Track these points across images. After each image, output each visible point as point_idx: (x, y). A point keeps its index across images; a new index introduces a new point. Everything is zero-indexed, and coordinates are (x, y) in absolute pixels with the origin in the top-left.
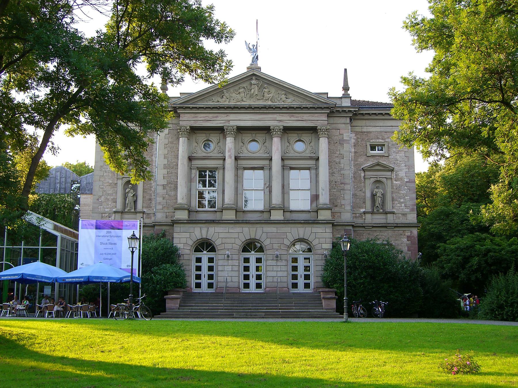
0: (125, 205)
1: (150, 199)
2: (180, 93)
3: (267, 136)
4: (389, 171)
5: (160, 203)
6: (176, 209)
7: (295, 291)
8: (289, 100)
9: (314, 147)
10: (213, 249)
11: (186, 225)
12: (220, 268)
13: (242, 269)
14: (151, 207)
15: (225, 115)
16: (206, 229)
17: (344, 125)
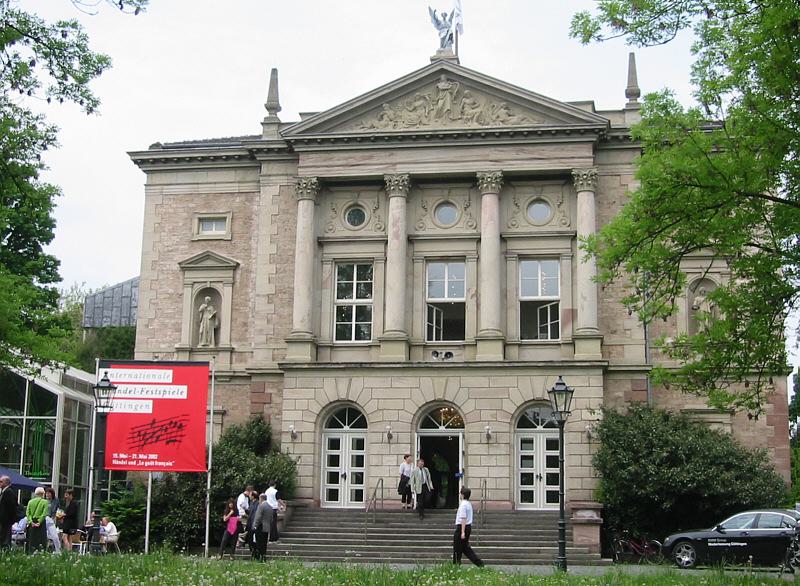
0: (196, 336)
1: (245, 324)
2: (300, 114)
3: (382, 195)
4: (227, 268)
5: (261, 330)
6: (289, 342)
7: (527, 507)
8: (514, 119)
9: (567, 214)
10: (362, 423)
11: (308, 374)
12: (374, 460)
13: (324, 461)
14: (246, 340)
15: (388, 153)
16: (346, 380)
17: (628, 166)
